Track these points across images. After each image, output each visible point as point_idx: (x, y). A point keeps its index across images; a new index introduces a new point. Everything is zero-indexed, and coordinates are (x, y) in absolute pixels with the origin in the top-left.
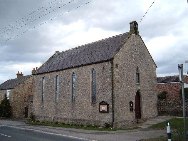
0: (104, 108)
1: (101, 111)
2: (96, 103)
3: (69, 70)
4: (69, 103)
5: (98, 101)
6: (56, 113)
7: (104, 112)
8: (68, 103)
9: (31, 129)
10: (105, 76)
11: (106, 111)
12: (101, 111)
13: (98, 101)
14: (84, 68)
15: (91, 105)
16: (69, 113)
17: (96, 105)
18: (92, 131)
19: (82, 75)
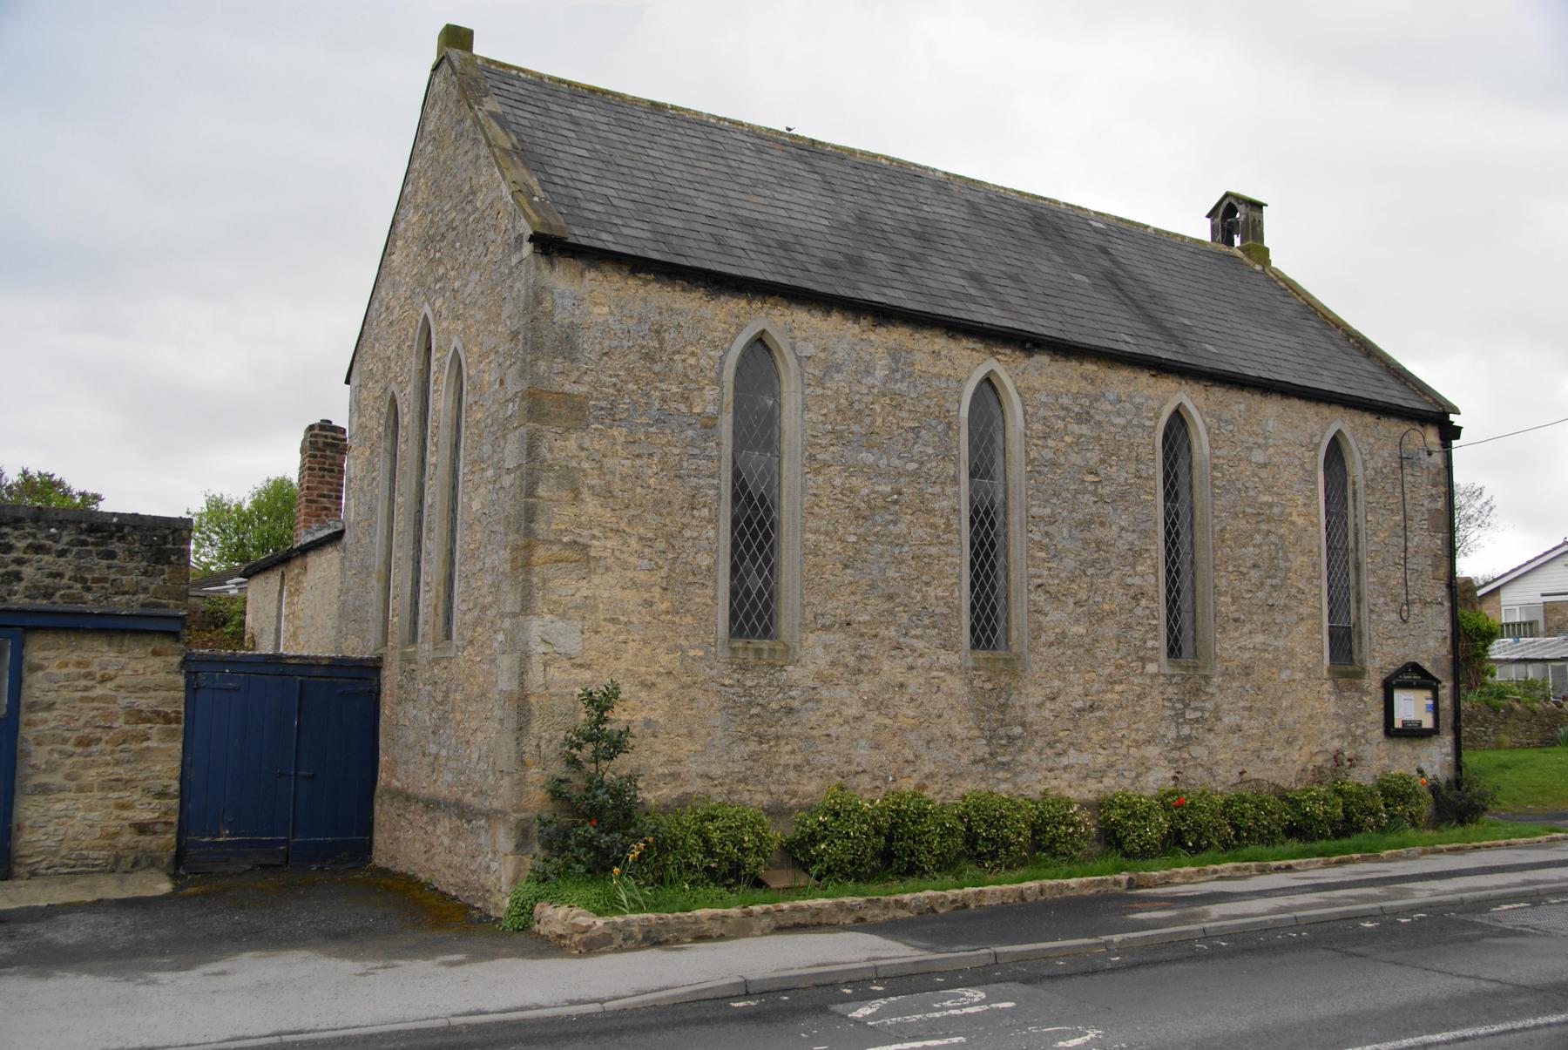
0: (1411, 707)
1: (1398, 725)
2: (1360, 674)
3: (1144, 378)
4: (1151, 668)
5: (1380, 657)
6: (990, 762)
7: (1413, 733)
8: (1143, 660)
9: (1474, 1038)
10: (1410, 512)
11: (1428, 723)
12: (1398, 725)
13: (1380, 657)
14: (1271, 409)
15: (1328, 686)
16: (1152, 751)
17: (1366, 682)
18: (731, 386)
19: (1258, 456)
